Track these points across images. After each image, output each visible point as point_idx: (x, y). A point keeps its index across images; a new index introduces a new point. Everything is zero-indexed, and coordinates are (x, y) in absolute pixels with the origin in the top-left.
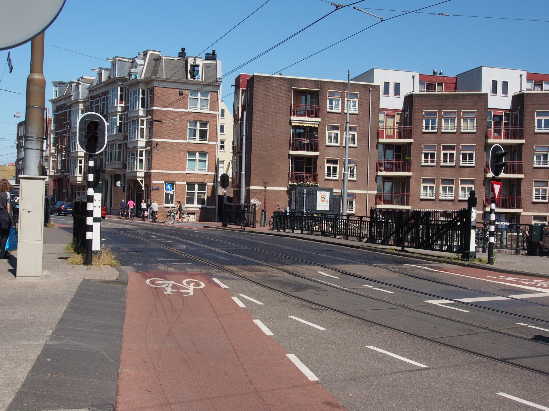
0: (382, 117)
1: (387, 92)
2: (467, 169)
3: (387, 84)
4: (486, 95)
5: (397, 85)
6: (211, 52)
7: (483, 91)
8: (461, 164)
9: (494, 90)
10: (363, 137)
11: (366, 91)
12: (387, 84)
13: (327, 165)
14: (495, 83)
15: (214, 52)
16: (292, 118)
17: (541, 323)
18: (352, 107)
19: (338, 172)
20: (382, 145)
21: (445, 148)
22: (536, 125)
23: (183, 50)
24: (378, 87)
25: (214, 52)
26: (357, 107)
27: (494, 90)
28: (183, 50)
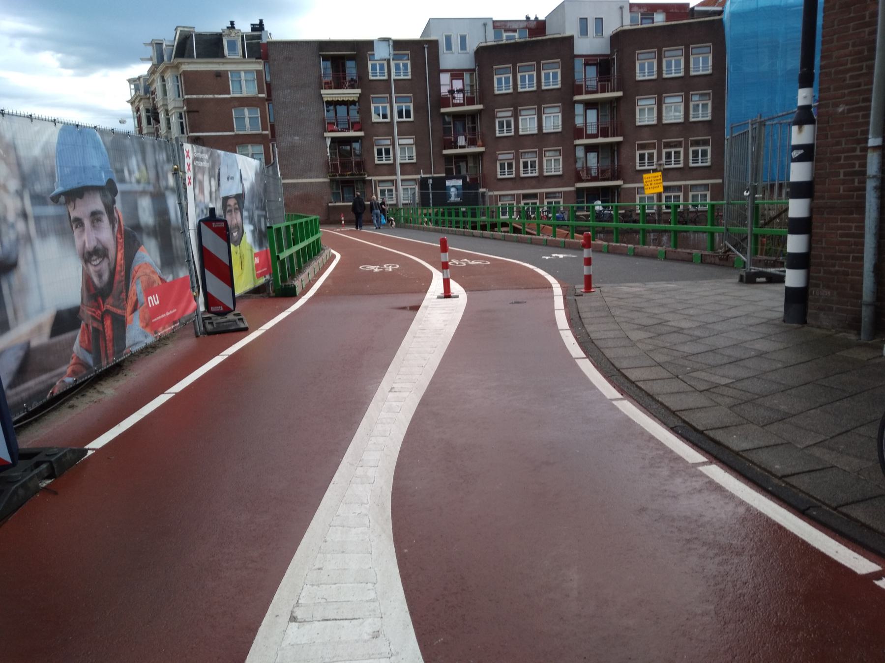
0: (445, 78)
1: (449, 47)
2: (552, 136)
3: (448, 39)
4: (571, 39)
5: (463, 39)
6: (258, 22)
7: (568, 34)
8: (691, 165)
9: (584, 31)
10: (420, 108)
12: (448, 39)
14: (584, 21)
15: (261, 21)
16: (323, 92)
17: (184, 203)
19: (391, 155)
20: (582, 148)
21: (668, 145)
23: (232, 23)
25: (261, 21)
26: (409, 70)
27: (584, 31)
28: (232, 23)
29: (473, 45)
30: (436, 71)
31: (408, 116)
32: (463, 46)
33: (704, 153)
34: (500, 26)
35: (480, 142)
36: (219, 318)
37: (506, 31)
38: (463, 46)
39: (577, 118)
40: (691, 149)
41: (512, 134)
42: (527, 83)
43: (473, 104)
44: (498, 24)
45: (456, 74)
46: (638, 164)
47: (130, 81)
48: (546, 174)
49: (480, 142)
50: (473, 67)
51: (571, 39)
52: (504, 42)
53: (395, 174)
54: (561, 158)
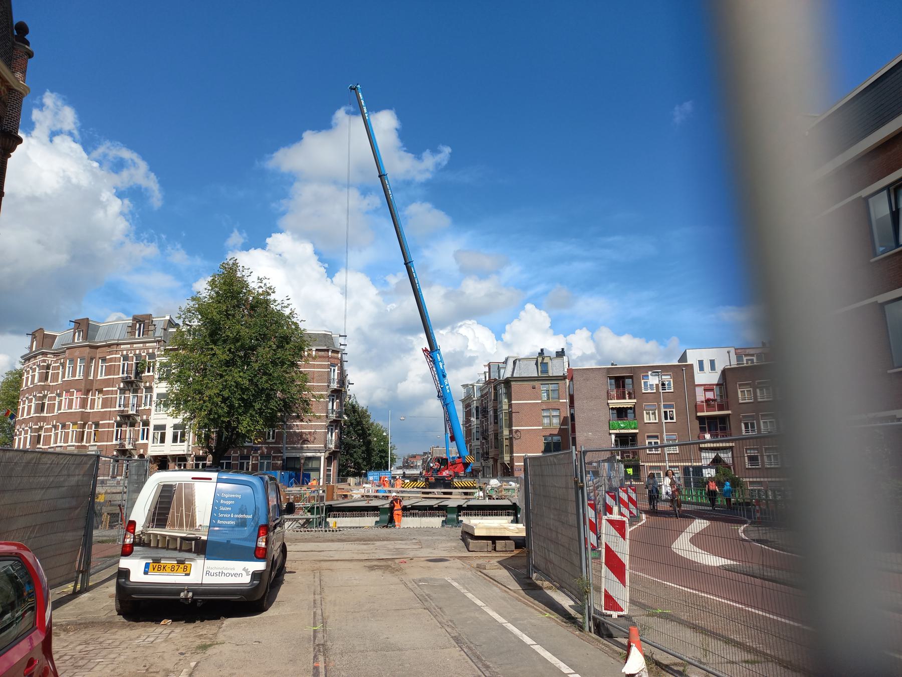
1: (701, 368)
3: (701, 363)
5: (712, 363)
11: (682, 371)
12: (701, 363)
22: (740, 396)
24: (692, 365)
29: (719, 367)
31: (672, 418)
32: (713, 367)
38: (713, 367)
45: (708, 388)
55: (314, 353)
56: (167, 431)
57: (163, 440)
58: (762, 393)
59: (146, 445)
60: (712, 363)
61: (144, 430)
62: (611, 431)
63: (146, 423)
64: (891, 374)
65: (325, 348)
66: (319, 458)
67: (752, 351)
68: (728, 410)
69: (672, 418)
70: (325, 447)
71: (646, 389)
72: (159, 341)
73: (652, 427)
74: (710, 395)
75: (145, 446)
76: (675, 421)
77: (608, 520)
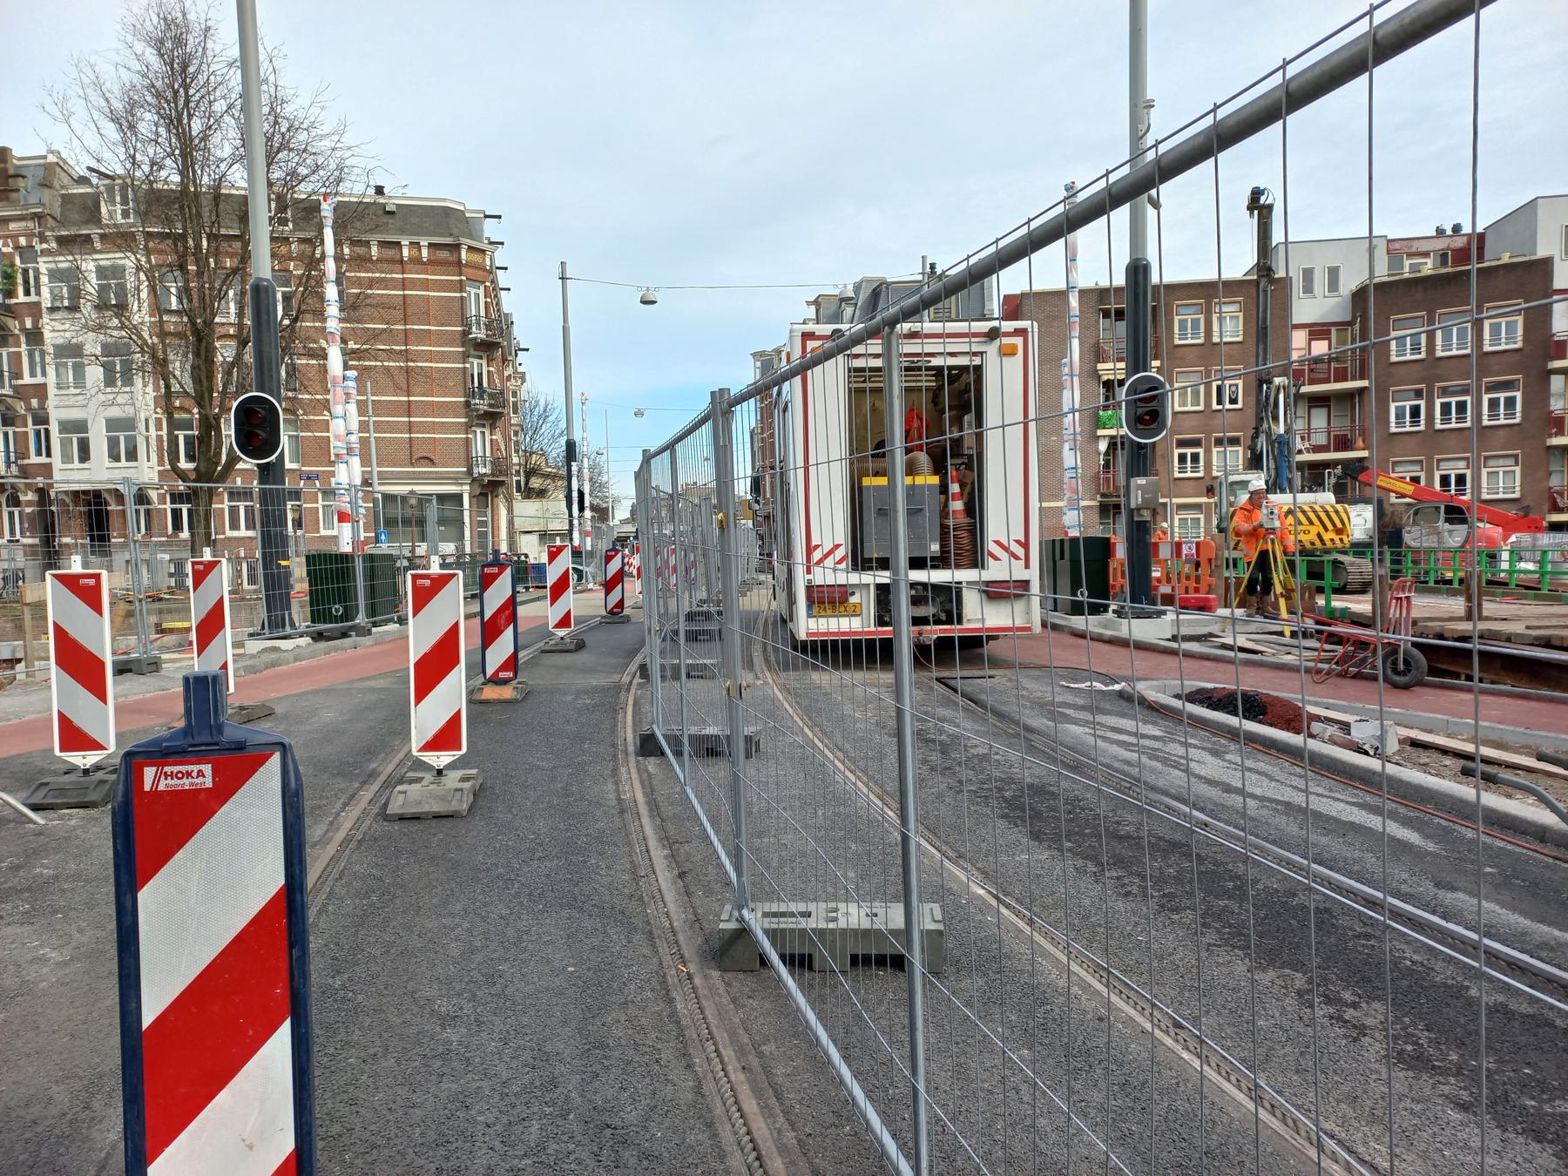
0: (1299, 339)
1: (1308, 289)
2: (1501, 432)
4: (1547, 263)
5: (1334, 273)
7: (1541, 253)
12: (1308, 274)
13: (1177, 452)
18: (1230, 325)
21: (1445, 392)
29: (1350, 282)
30: (1287, 326)
31: (1233, 401)
32: (1333, 284)
33: (1510, 402)
34: (1398, 249)
35: (1360, 443)
36: (869, 291)
37: (1410, 255)
38: (1333, 284)
39: (1552, 401)
40: (1486, 398)
41: (1422, 427)
42: (1452, 342)
43: (1345, 379)
44: (1397, 246)
45: (1318, 331)
46: (1438, 421)
47: (754, 355)
48: (1485, 496)
49: (1360, 443)
50: (1349, 318)
51: (1547, 263)
52: (1407, 275)
53: (1470, 652)
54: (1518, 469)
55: (425, 253)
56: (91, 435)
57: (85, 454)
58: (1447, 338)
59: (49, 467)
60: (1334, 273)
61: (38, 433)
62: (1100, 432)
63: (41, 419)
64: (1085, 507)
65: (448, 240)
66: (458, 498)
67: (1424, 246)
68: (1362, 378)
69: (1233, 401)
70: (470, 472)
71: (1183, 336)
72: (38, 217)
73: (1189, 422)
74: (1320, 348)
75: (47, 470)
76: (1239, 406)
77: (97, 746)
